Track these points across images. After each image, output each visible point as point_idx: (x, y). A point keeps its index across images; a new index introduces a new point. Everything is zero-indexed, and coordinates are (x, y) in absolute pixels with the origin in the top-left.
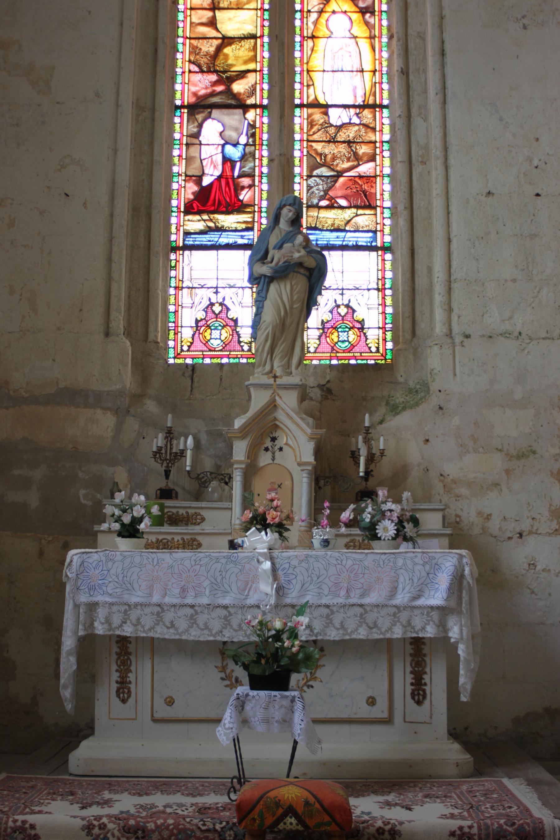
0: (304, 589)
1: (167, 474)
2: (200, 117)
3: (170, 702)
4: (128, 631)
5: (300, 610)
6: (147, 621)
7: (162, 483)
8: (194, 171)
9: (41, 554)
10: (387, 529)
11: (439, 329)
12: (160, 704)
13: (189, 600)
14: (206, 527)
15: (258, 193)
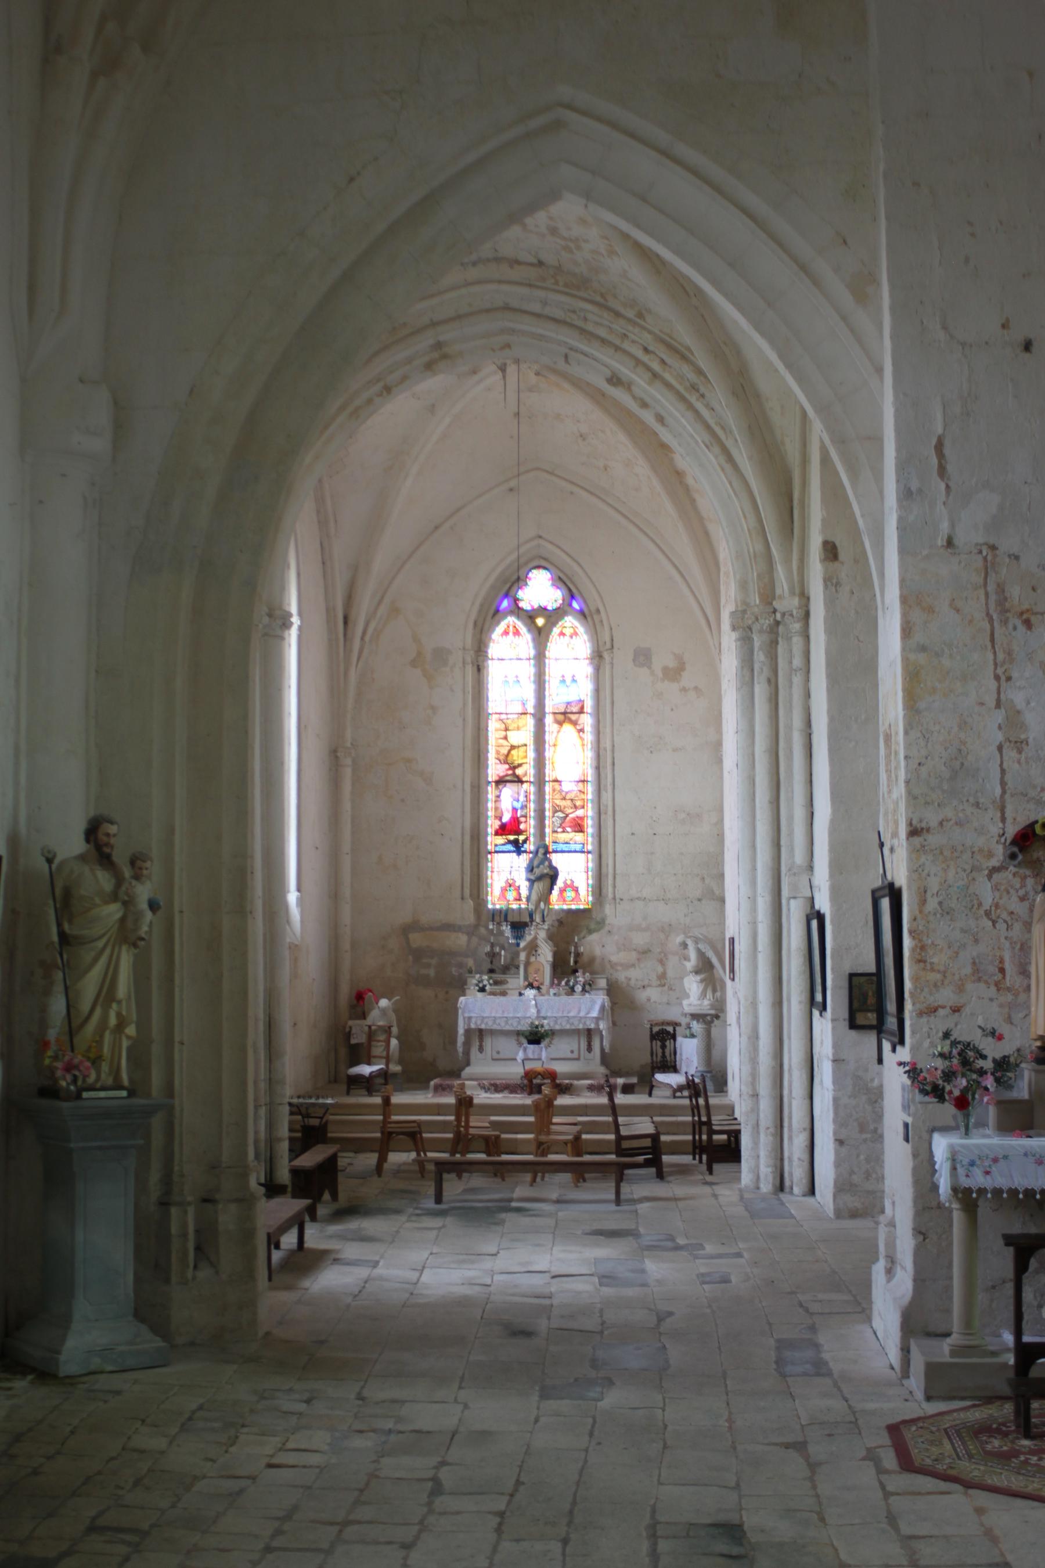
1: (491, 962)
3: (498, 1053)
4: (483, 1027)
5: (545, 1018)
6: (490, 1023)
7: (489, 966)
8: (498, 815)
9: (436, 996)
10: (578, 988)
11: (610, 896)
12: (494, 1054)
14: (509, 986)
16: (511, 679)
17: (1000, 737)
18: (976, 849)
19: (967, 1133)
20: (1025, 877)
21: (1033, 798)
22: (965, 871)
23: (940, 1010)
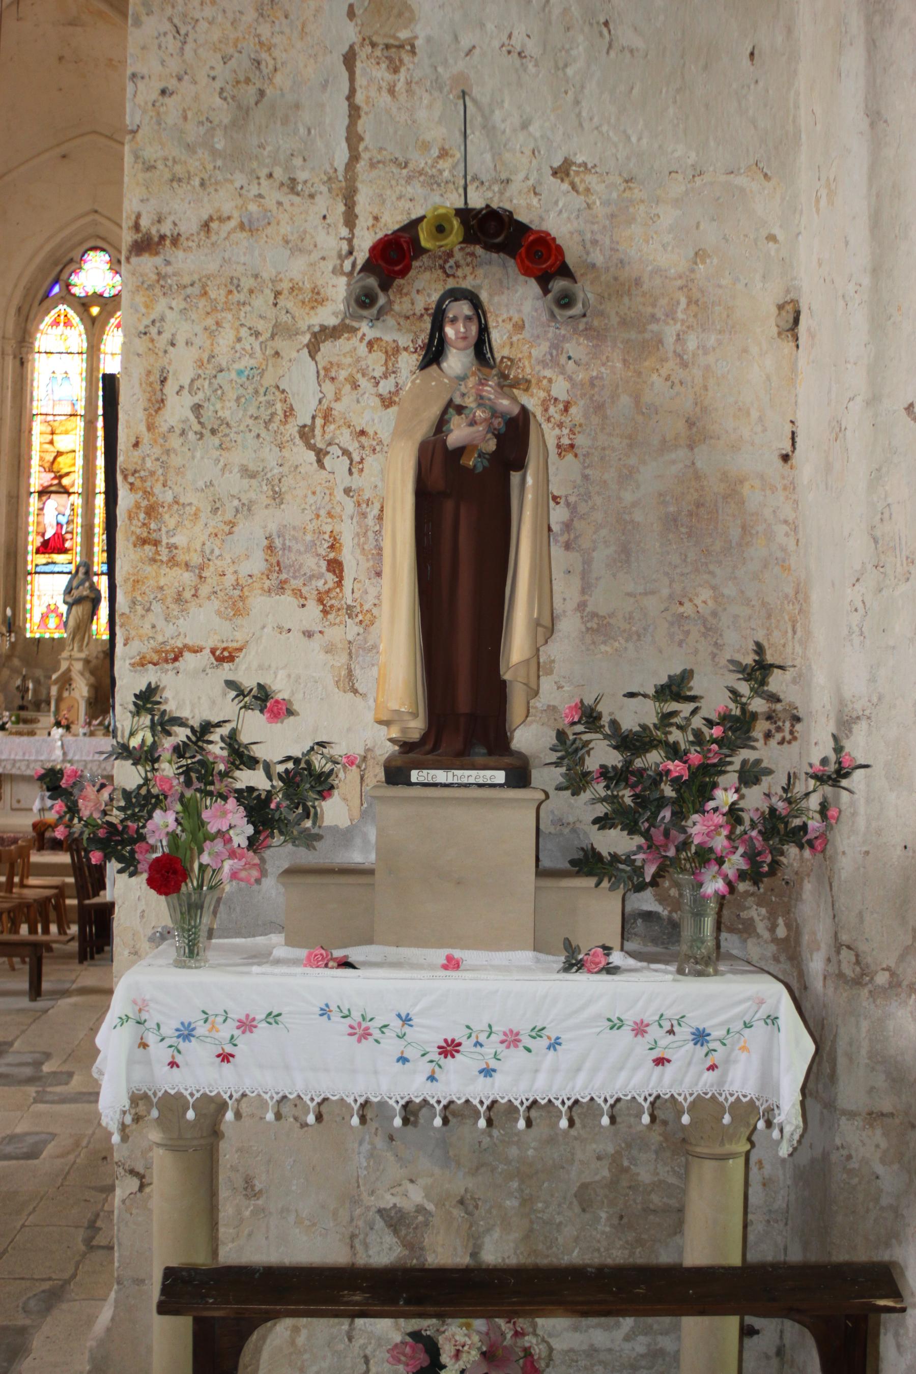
0: (75, 754)
1: (23, 698)
2: (44, 498)
3: (19, 801)
6: (9, 767)
8: (41, 530)
12: (14, 802)
13: (26, 758)
14: (39, 725)
15: (75, 542)
16: (59, 375)
17: (350, 33)
18: (285, 286)
19: (192, 952)
20: (397, 350)
21: (421, 173)
22: (257, 334)
23: (187, 655)
